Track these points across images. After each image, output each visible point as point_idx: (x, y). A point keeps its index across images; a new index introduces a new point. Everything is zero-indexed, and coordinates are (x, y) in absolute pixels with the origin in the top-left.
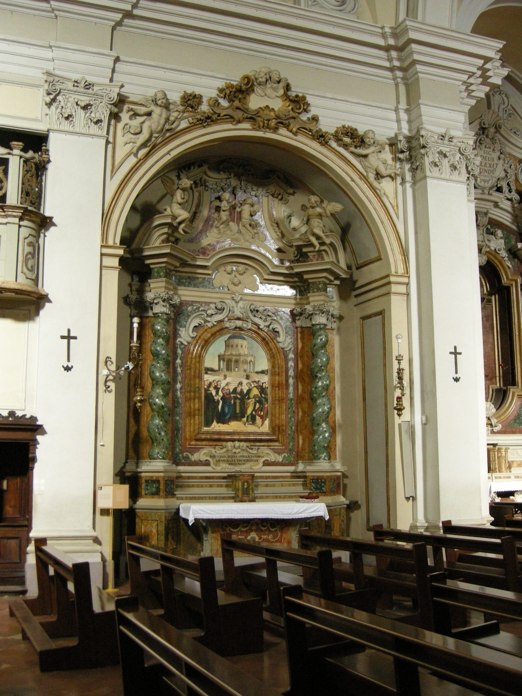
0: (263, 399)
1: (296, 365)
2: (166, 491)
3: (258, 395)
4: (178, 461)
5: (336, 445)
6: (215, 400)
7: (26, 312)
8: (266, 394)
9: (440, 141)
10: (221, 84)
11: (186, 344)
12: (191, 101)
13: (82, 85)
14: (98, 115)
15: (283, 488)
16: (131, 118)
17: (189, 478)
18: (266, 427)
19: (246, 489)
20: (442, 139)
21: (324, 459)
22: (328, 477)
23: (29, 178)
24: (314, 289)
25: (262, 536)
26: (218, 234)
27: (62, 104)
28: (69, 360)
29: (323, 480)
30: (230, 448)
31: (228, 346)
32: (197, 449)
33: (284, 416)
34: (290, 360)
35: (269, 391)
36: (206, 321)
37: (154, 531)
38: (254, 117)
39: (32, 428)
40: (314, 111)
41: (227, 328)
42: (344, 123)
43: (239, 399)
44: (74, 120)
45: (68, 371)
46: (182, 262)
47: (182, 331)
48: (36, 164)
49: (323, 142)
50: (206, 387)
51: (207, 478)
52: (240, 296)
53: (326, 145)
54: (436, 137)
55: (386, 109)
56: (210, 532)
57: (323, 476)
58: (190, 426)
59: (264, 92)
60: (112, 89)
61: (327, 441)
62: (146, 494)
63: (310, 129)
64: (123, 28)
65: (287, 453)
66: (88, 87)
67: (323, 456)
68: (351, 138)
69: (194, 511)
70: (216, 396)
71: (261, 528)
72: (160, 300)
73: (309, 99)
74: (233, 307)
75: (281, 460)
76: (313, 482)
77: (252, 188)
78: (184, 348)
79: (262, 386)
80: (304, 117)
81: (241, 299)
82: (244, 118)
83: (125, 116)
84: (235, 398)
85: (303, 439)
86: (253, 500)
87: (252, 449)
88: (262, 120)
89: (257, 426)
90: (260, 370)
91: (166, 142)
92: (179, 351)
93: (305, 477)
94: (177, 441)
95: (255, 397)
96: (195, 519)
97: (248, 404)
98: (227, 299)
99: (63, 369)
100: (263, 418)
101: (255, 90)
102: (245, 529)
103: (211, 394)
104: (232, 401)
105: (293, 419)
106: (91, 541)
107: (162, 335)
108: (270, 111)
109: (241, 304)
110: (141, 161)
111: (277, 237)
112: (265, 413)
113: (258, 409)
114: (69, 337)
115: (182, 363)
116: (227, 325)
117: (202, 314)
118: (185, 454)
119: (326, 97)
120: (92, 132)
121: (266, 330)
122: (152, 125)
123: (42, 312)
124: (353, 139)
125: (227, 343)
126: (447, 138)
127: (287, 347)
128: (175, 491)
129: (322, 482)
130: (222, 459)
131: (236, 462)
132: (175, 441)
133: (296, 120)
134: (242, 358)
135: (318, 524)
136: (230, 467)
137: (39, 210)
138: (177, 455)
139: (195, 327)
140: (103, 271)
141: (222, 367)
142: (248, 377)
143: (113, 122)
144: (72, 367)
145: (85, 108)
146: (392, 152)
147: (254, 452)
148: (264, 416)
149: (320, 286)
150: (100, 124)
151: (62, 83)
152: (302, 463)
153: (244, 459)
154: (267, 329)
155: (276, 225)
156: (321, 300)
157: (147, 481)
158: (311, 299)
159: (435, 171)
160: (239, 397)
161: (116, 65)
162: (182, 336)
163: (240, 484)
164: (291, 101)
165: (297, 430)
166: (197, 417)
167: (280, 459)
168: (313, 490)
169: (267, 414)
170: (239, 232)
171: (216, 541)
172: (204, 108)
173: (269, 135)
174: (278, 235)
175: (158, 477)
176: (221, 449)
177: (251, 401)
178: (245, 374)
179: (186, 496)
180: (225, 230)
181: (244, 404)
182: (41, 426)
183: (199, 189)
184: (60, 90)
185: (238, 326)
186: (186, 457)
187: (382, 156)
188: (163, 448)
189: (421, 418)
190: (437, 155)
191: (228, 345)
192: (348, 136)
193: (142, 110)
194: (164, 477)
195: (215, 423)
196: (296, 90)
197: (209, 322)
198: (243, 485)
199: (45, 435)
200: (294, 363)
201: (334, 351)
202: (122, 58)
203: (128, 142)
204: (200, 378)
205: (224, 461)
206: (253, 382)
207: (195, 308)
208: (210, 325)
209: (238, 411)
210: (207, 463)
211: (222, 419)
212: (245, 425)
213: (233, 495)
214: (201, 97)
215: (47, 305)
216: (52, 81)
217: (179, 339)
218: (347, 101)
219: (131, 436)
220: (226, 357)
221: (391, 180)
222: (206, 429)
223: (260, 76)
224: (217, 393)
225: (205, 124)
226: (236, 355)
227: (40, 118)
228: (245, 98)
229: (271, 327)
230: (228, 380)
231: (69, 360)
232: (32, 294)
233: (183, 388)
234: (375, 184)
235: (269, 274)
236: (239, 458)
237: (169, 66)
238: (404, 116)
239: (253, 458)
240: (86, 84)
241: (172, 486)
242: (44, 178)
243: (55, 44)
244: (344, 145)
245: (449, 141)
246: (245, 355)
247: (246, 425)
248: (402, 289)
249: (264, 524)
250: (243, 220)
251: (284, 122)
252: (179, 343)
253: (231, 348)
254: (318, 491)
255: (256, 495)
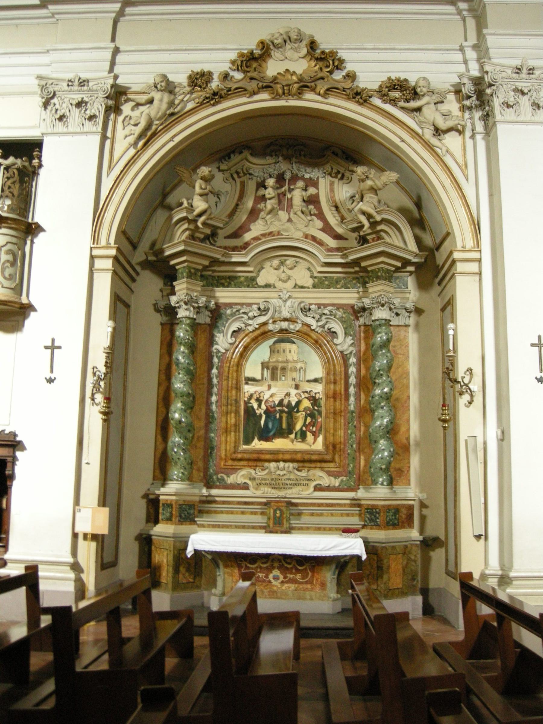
0: (316, 413)
1: (359, 370)
2: (180, 516)
3: (309, 407)
4: (211, 484)
5: (409, 467)
6: (256, 413)
7: (14, 323)
8: (320, 406)
9: (515, 75)
10: (233, 55)
11: (224, 351)
12: (199, 80)
13: (76, 83)
14: (93, 111)
15: (333, 518)
16: (133, 109)
17: (224, 503)
18: (319, 445)
19: (279, 518)
20: (518, 73)
21: (382, 484)
22: (383, 506)
23: (10, 185)
24: (373, 278)
25: (288, 575)
26: (264, 226)
27: (57, 106)
28: (52, 371)
29: (377, 510)
30: (273, 470)
31: (274, 352)
32: (234, 470)
33: (342, 431)
34: (351, 365)
35: (323, 403)
36: (247, 325)
37: (165, 561)
38: (271, 84)
39: (13, 444)
40: (349, 67)
41: (271, 331)
42: (389, 75)
43: (286, 412)
44: (68, 120)
45: (50, 383)
46: (212, 260)
47: (219, 338)
48: (19, 170)
49: (361, 101)
50: (246, 399)
51: (246, 503)
52: (289, 293)
53: (365, 104)
54: (509, 71)
55: (447, 50)
56: (221, 566)
57: (377, 505)
58: (225, 444)
59: (282, 54)
60: (105, 81)
61: (385, 462)
62: (162, 520)
63: (344, 88)
64: (127, 18)
65: (346, 476)
66: (82, 84)
67: (381, 479)
68: (401, 91)
69: (204, 540)
70: (258, 409)
71: (286, 565)
72: (182, 303)
73: (342, 54)
74: (280, 307)
75: (337, 484)
76: (367, 512)
77: (305, 171)
78: (221, 355)
79: (315, 397)
80: (338, 76)
81: (290, 297)
82: (259, 88)
83: (126, 109)
84: (282, 411)
85: (365, 460)
86: (288, 531)
87: (301, 471)
88: (281, 86)
89: (308, 444)
90: (312, 377)
91: (167, 128)
92: (216, 360)
93: (359, 506)
94: (211, 460)
95: (305, 409)
96: (196, 551)
97: (297, 418)
98: (273, 298)
100: (315, 435)
101: (272, 54)
102: (265, 566)
103: (252, 407)
104: (278, 415)
105: (354, 435)
106: (69, 568)
107: (183, 342)
108: (292, 75)
109: (289, 303)
110: (139, 153)
111: (337, 222)
112: (318, 428)
113: (309, 423)
114: (53, 347)
115: (219, 373)
116: (271, 327)
117: (243, 317)
118: (219, 476)
119: (365, 49)
120: (86, 129)
121: (319, 330)
122: (151, 112)
123: (27, 322)
124: (402, 92)
125: (272, 348)
126: (525, 71)
127: (347, 350)
128: (197, 517)
129: (377, 513)
130: (263, 482)
131: (281, 486)
132: (209, 461)
133: (326, 80)
134: (290, 365)
135: (370, 563)
136: (273, 491)
137: (27, 217)
138: (211, 477)
139: (234, 331)
140: (96, 275)
141: (265, 376)
142: (297, 387)
143: (112, 116)
144: (55, 378)
145: (79, 105)
146: (459, 101)
147: (303, 474)
148: (317, 432)
149: (379, 274)
150: (95, 120)
151: (57, 85)
152: (364, 488)
153: (290, 482)
154: (321, 329)
155: (334, 209)
156: (380, 291)
157: (163, 505)
158: (370, 290)
159: (510, 114)
160: (286, 410)
162: (219, 343)
163: (272, 511)
164: (317, 59)
165: (359, 449)
166: (233, 433)
167: (336, 482)
168: (368, 521)
169: (320, 430)
170: (290, 220)
171: (231, 578)
172: (215, 84)
174: (337, 220)
175: (172, 500)
176: (262, 470)
177: (301, 416)
178: (294, 383)
179: (209, 523)
180: (272, 220)
181: (292, 418)
182: (20, 442)
183: (242, 179)
184: (54, 92)
185: (284, 328)
186: (220, 479)
187: (443, 108)
188: (181, 468)
189: (497, 432)
190: (512, 93)
191: (273, 350)
192: (397, 89)
193: (143, 98)
194: (177, 501)
195: (256, 441)
196: (325, 44)
197: (250, 325)
198: (275, 511)
199: (25, 451)
200: (357, 369)
201: (408, 351)
202: (122, 48)
203: (128, 134)
204: (238, 388)
205: (266, 484)
206: (303, 392)
207: (234, 310)
208: (251, 329)
209: (284, 426)
210: (245, 487)
211: (265, 436)
212: (293, 443)
213: (264, 525)
214: (210, 74)
215: (32, 314)
216: (44, 84)
217: (216, 346)
218: (394, 49)
219: (158, 455)
220: (271, 365)
221: (457, 134)
222: (245, 447)
223: (274, 37)
224: (259, 406)
225: (212, 102)
226: (282, 362)
227: (38, 125)
228: (260, 66)
229: (326, 327)
230: (273, 390)
231: (52, 371)
232: (8, 303)
233: (219, 401)
234: (434, 141)
235: (322, 266)
236: (284, 482)
237: (173, 47)
238: (471, 55)
239: (302, 482)
240: (80, 81)
241: (192, 512)
242: (34, 184)
243: (51, 48)
244: (391, 100)
245: (529, 74)
246: (294, 361)
247: (295, 442)
248: (473, 267)
249: (289, 561)
250: (294, 207)
251: (309, 84)
252: (215, 351)
253: (276, 354)
254: (372, 524)
255: (294, 525)
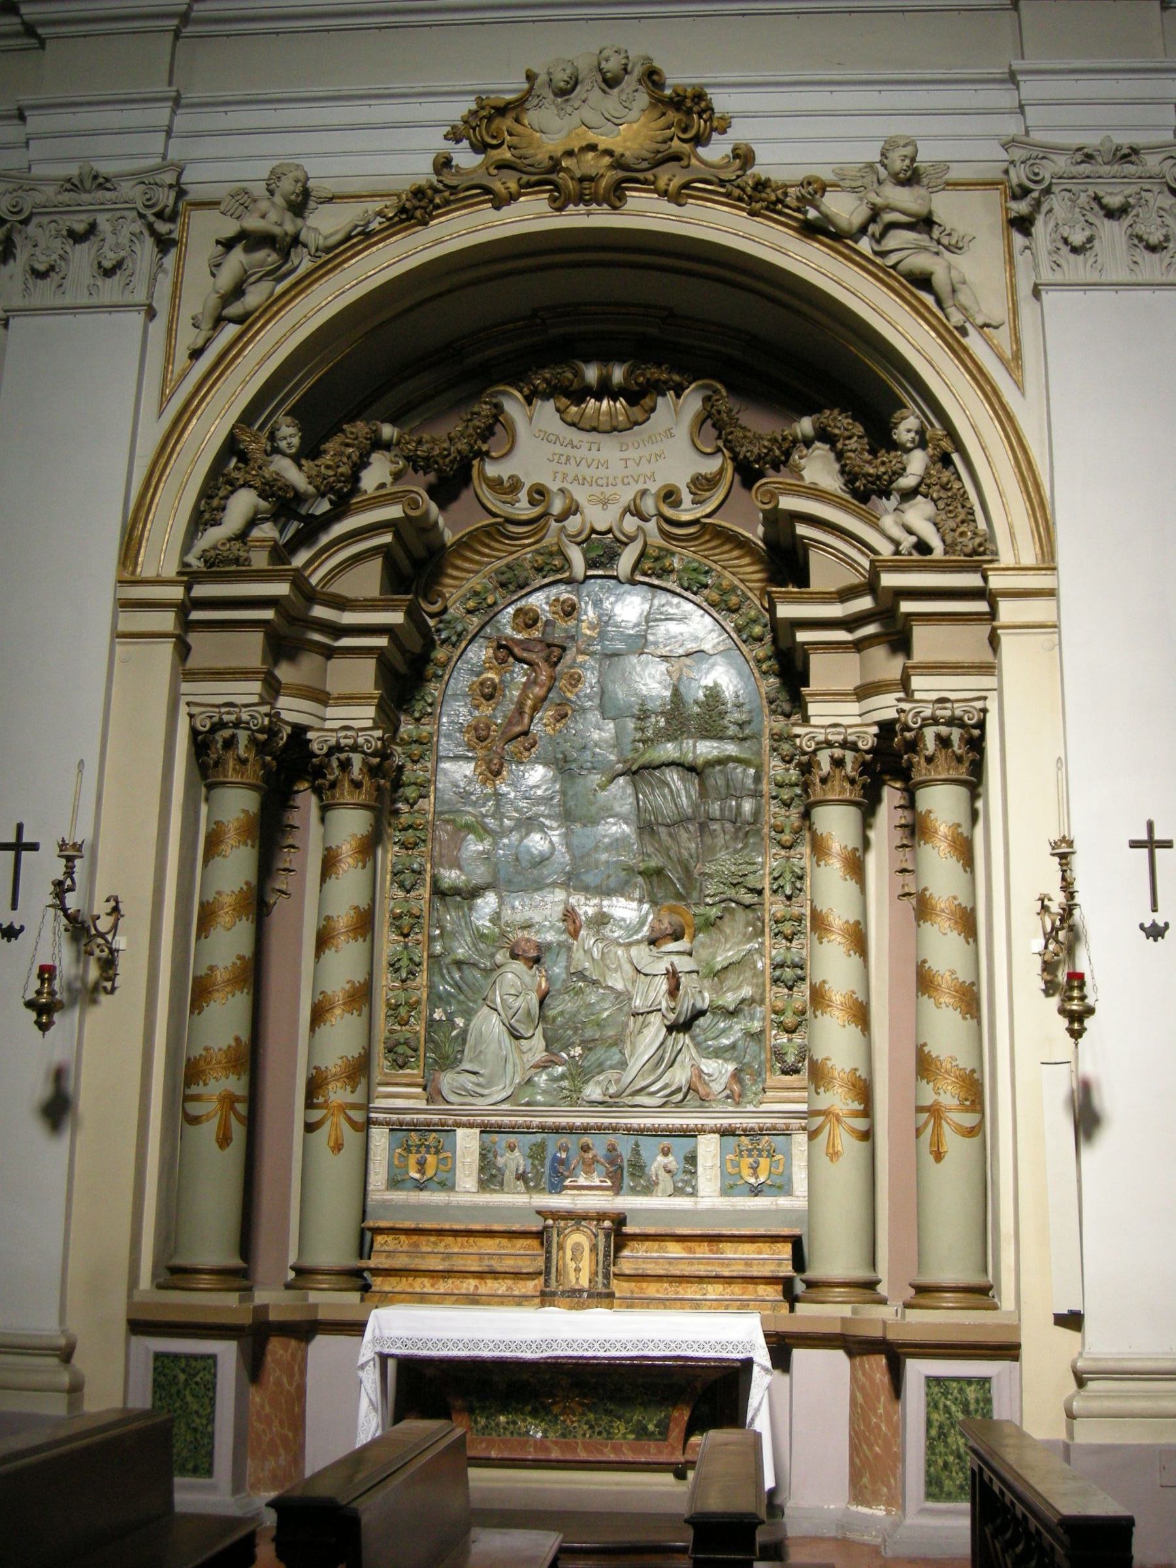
10: (458, 109)
73: (721, 102)
99: (1143, 934)
144: (1167, 925)
161: (177, 119)
173: (601, 219)
196: (677, 77)
